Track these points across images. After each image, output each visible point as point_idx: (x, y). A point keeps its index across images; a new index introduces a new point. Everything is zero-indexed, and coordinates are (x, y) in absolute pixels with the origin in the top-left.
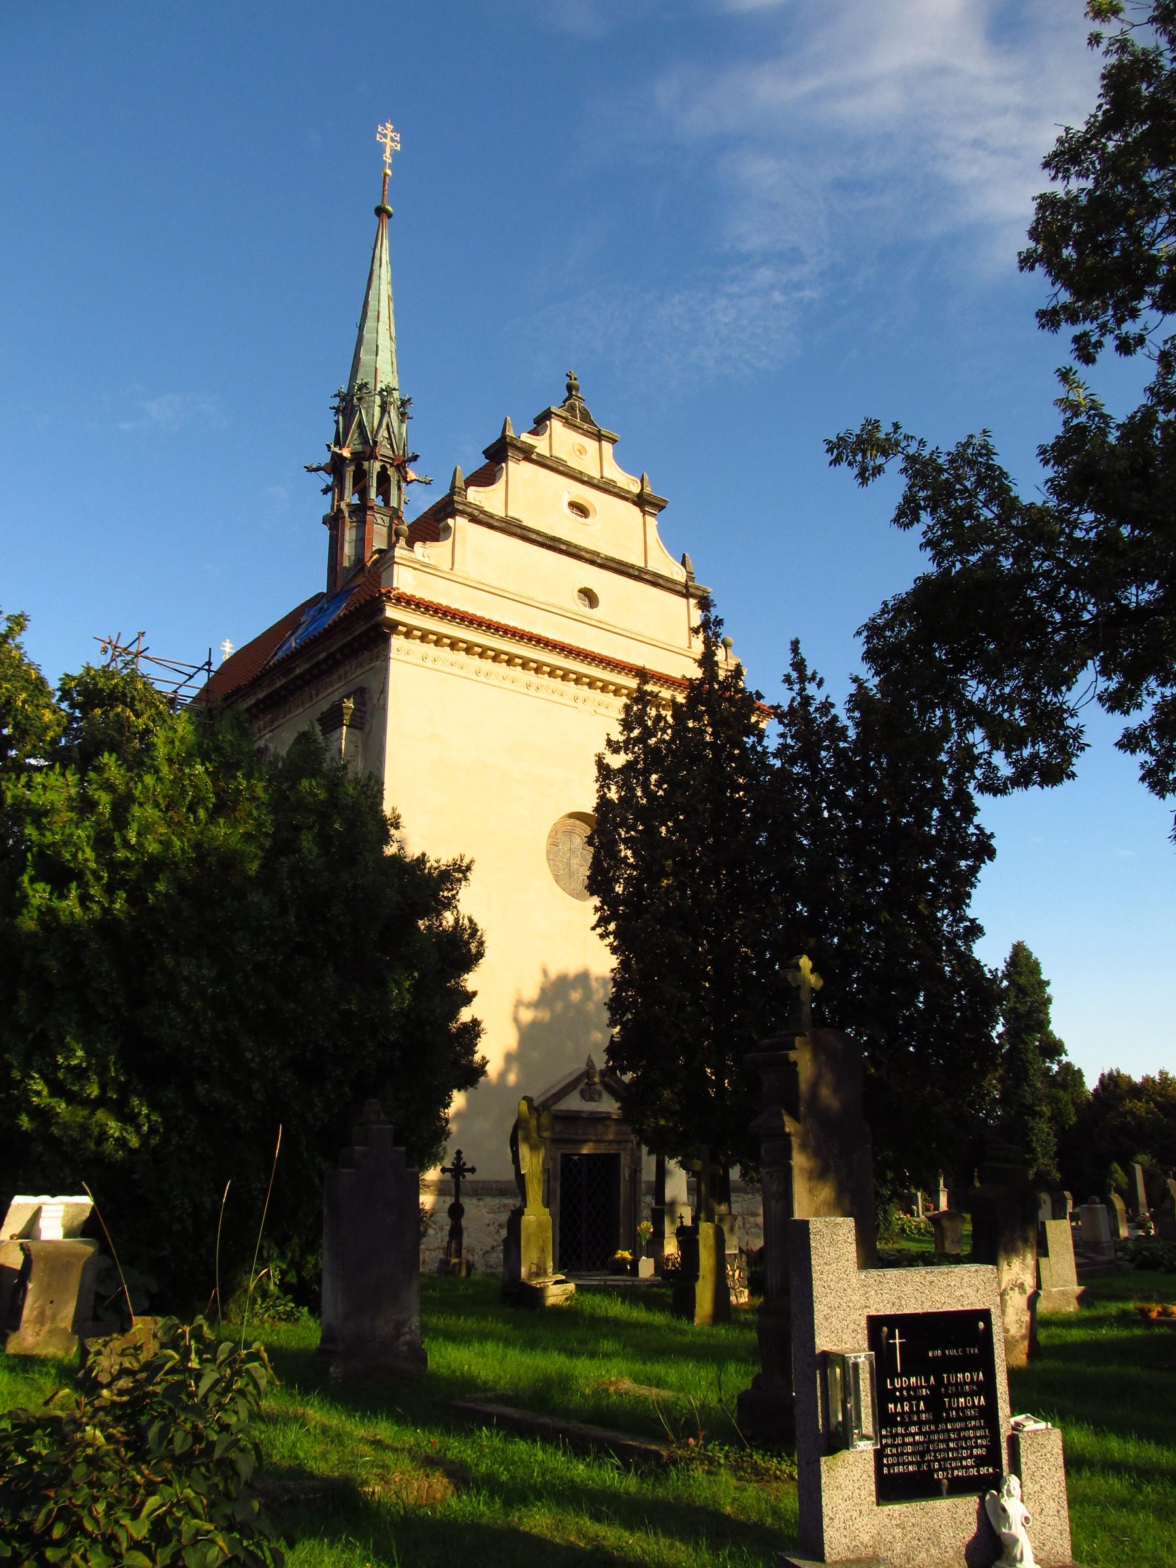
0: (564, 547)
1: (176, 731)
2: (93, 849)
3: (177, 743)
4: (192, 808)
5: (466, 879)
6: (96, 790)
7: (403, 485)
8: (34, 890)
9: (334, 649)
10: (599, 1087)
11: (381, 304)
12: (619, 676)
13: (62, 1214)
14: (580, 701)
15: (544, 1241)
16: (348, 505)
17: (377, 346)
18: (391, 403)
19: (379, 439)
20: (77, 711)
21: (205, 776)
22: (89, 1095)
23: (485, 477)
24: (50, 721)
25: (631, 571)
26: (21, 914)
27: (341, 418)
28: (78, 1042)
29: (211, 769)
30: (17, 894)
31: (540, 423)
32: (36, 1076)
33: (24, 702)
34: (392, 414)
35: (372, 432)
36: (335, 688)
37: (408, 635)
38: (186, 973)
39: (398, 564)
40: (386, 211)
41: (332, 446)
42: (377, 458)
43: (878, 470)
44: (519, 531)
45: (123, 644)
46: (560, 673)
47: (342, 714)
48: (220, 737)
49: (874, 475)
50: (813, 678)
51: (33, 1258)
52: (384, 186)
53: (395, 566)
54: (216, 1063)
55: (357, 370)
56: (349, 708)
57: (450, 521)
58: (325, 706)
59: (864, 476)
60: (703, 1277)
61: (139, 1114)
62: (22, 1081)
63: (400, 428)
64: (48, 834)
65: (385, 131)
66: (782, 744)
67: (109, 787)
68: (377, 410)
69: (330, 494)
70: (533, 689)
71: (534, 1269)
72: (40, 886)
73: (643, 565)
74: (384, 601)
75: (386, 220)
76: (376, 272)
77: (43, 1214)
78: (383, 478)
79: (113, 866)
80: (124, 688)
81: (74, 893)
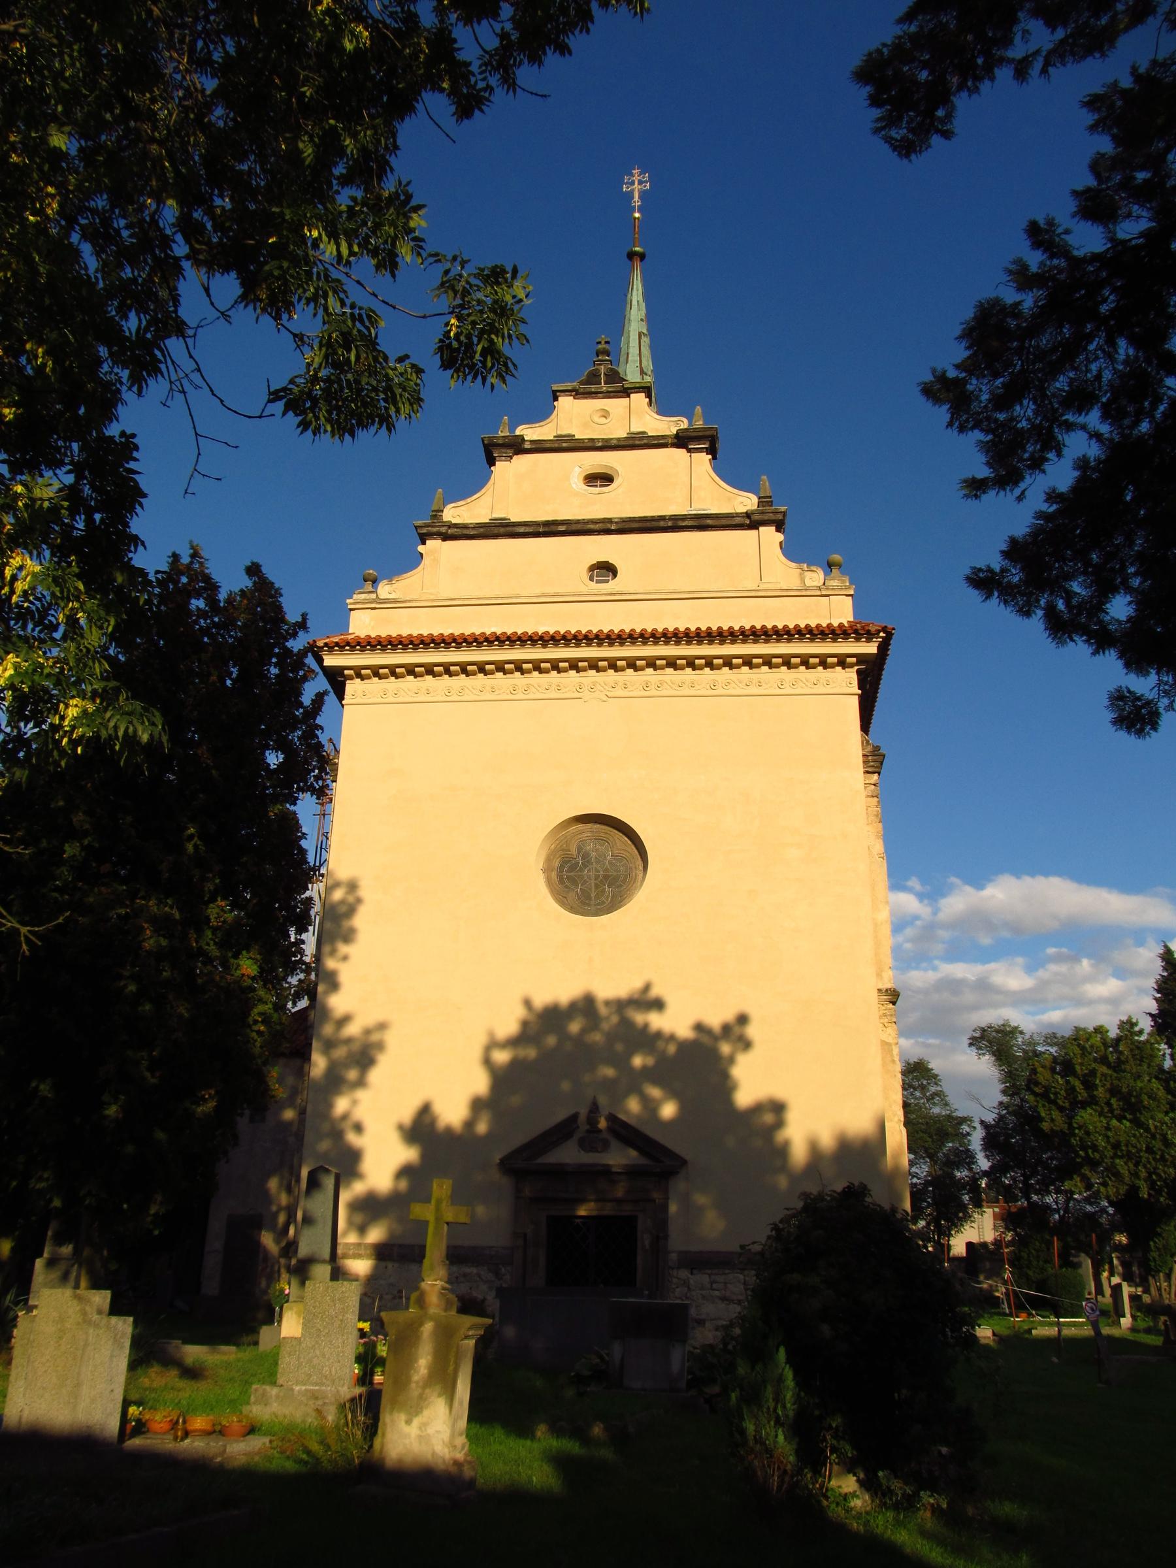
25: (662, 524)
44: (502, 530)
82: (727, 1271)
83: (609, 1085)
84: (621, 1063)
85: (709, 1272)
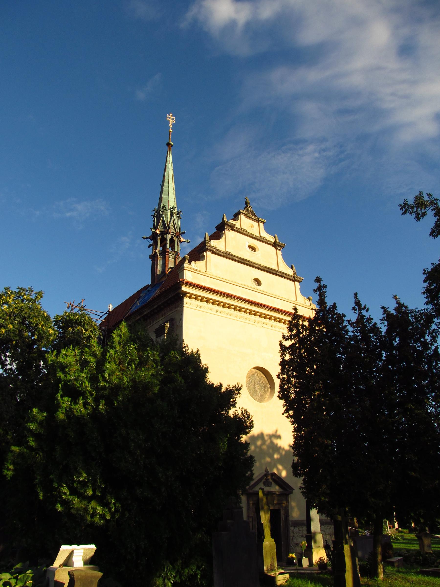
0: (247, 263)
1: (121, 331)
2: (89, 382)
3: (122, 336)
4: (129, 364)
5: (239, 393)
6: (88, 356)
7: (179, 243)
8: (63, 400)
9: (160, 303)
10: (271, 480)
11: (170, 177)
12: (271, 312)
13: (82, 554)
14: (256, 322)
15: (273, 554)
16: (159, 251)
17: (169, 192)
18: (174, 213)
19: (170, 226)
20: (61, 329)
21: (134, 350)
22: (88, 494)
23: (217, 236)
24: (52, 333)
26: (58, 411)
27: (155, 219)
28: (83, 470)
29: (137, 347)
30: (56, 402)
31: (236, 217)
32: (64, 485)
33: (42, 325)
34: (175, 217)
35: (167, 224)
36: (160, 319)
37: (190, 297)
38: (132, 438)
39: (186, 270)
40: (171, 144)
41: (153, 229)
42: (169, 233)
43: (424, 214)
44: (231, 257)
45: (75, 304)
46: (248, 311)
47: (165, 329)
48: (139, 333)
49: (422, 216)
50: (365, 307)
51: (75, 579)
52: (170, 136)
53: (185, 270)
54: (146, 479)
55: (161, 201)
56: (167, 327)
57: (205, 253)
58: (157, 326)
59: (418, 218)
60: (348, 571)
61: (111, 503)
62: (58, 487)
63: (178, 222)
64: (68, 376)
65: (170, 117)
66: (353, 335)
67: (94, 355)
68: (169, 216)
69: (151, 247)
70: (238, 318)
71: (269, 567)
72: (66, 399)
73: (277, 269)
74: (181, 284)
75: (170, 147)
76: (167, 166)
77: (74, 554)
78: (172, 241)
79: (98, 389)
80: (81, 319)
81: (81, 402)
82: (303, 527)
83: (269, 463)
84: (271, 456)
85: (298, 527)
